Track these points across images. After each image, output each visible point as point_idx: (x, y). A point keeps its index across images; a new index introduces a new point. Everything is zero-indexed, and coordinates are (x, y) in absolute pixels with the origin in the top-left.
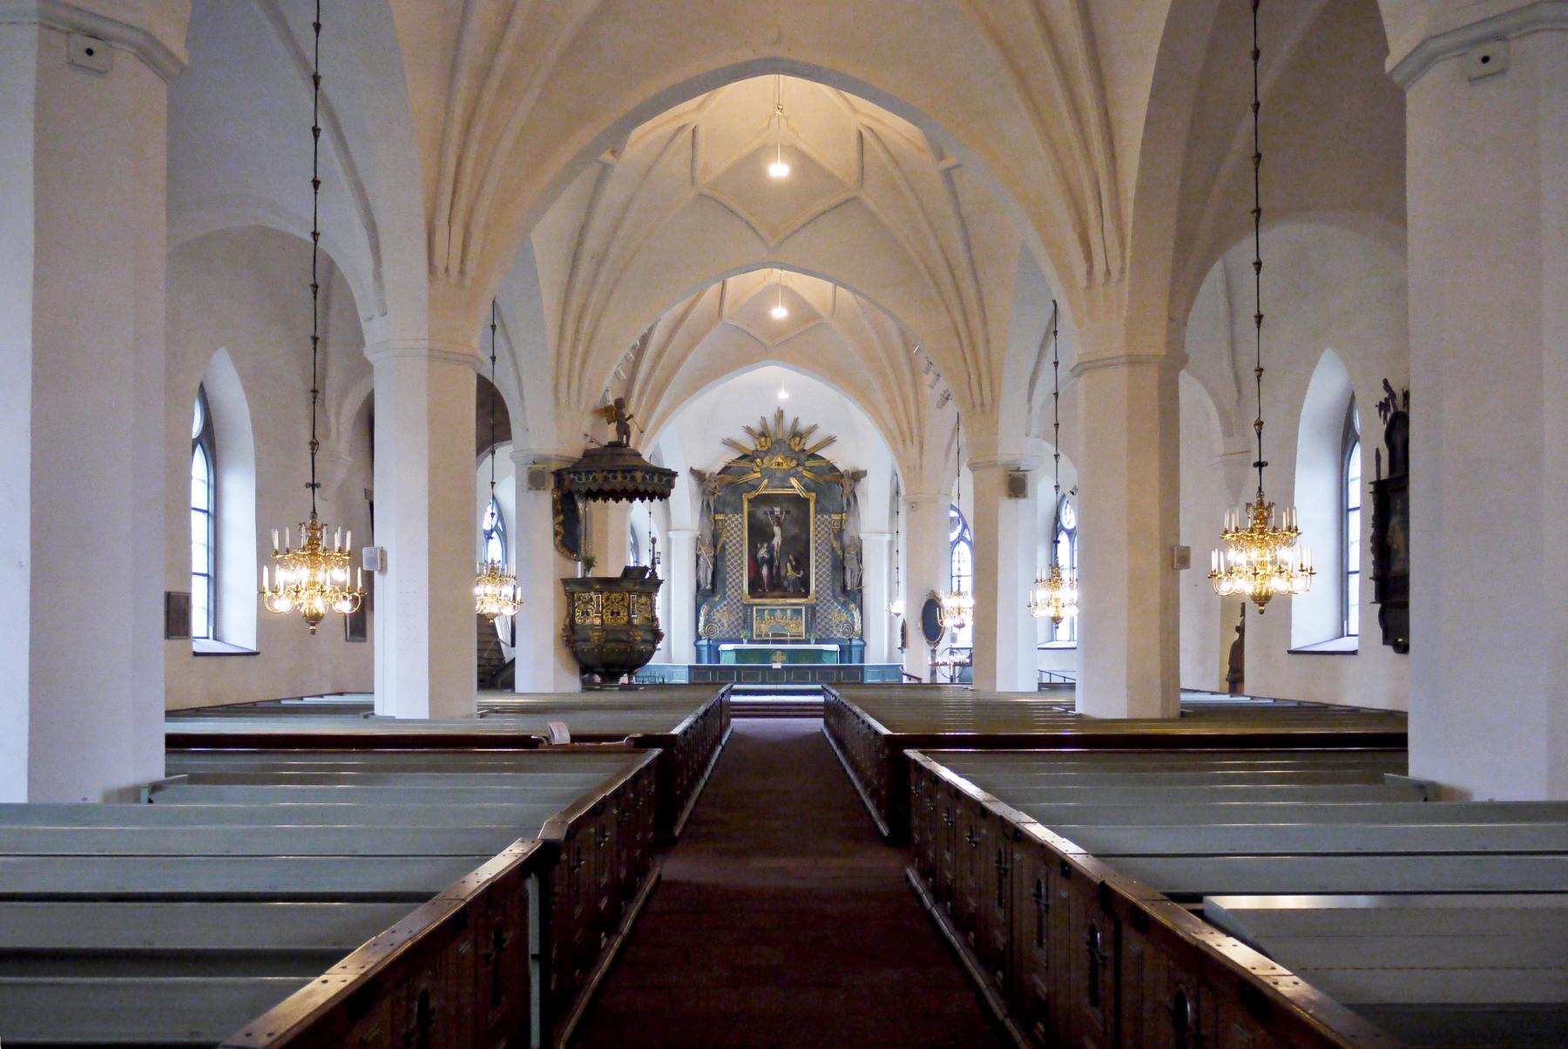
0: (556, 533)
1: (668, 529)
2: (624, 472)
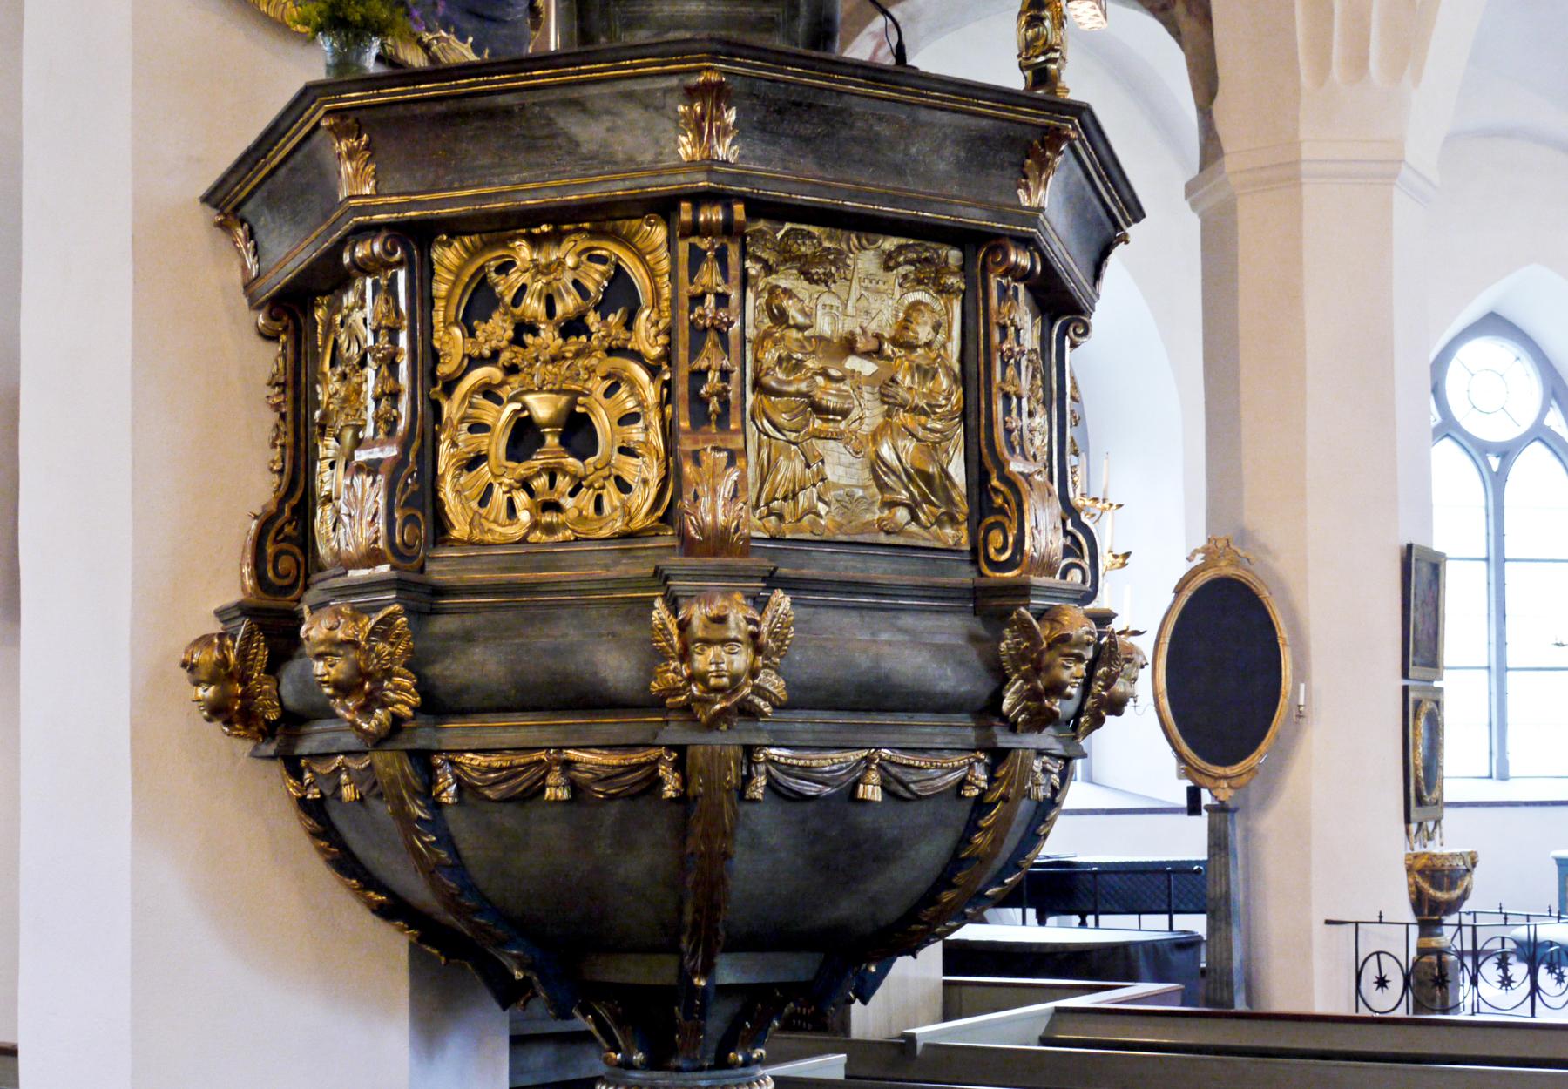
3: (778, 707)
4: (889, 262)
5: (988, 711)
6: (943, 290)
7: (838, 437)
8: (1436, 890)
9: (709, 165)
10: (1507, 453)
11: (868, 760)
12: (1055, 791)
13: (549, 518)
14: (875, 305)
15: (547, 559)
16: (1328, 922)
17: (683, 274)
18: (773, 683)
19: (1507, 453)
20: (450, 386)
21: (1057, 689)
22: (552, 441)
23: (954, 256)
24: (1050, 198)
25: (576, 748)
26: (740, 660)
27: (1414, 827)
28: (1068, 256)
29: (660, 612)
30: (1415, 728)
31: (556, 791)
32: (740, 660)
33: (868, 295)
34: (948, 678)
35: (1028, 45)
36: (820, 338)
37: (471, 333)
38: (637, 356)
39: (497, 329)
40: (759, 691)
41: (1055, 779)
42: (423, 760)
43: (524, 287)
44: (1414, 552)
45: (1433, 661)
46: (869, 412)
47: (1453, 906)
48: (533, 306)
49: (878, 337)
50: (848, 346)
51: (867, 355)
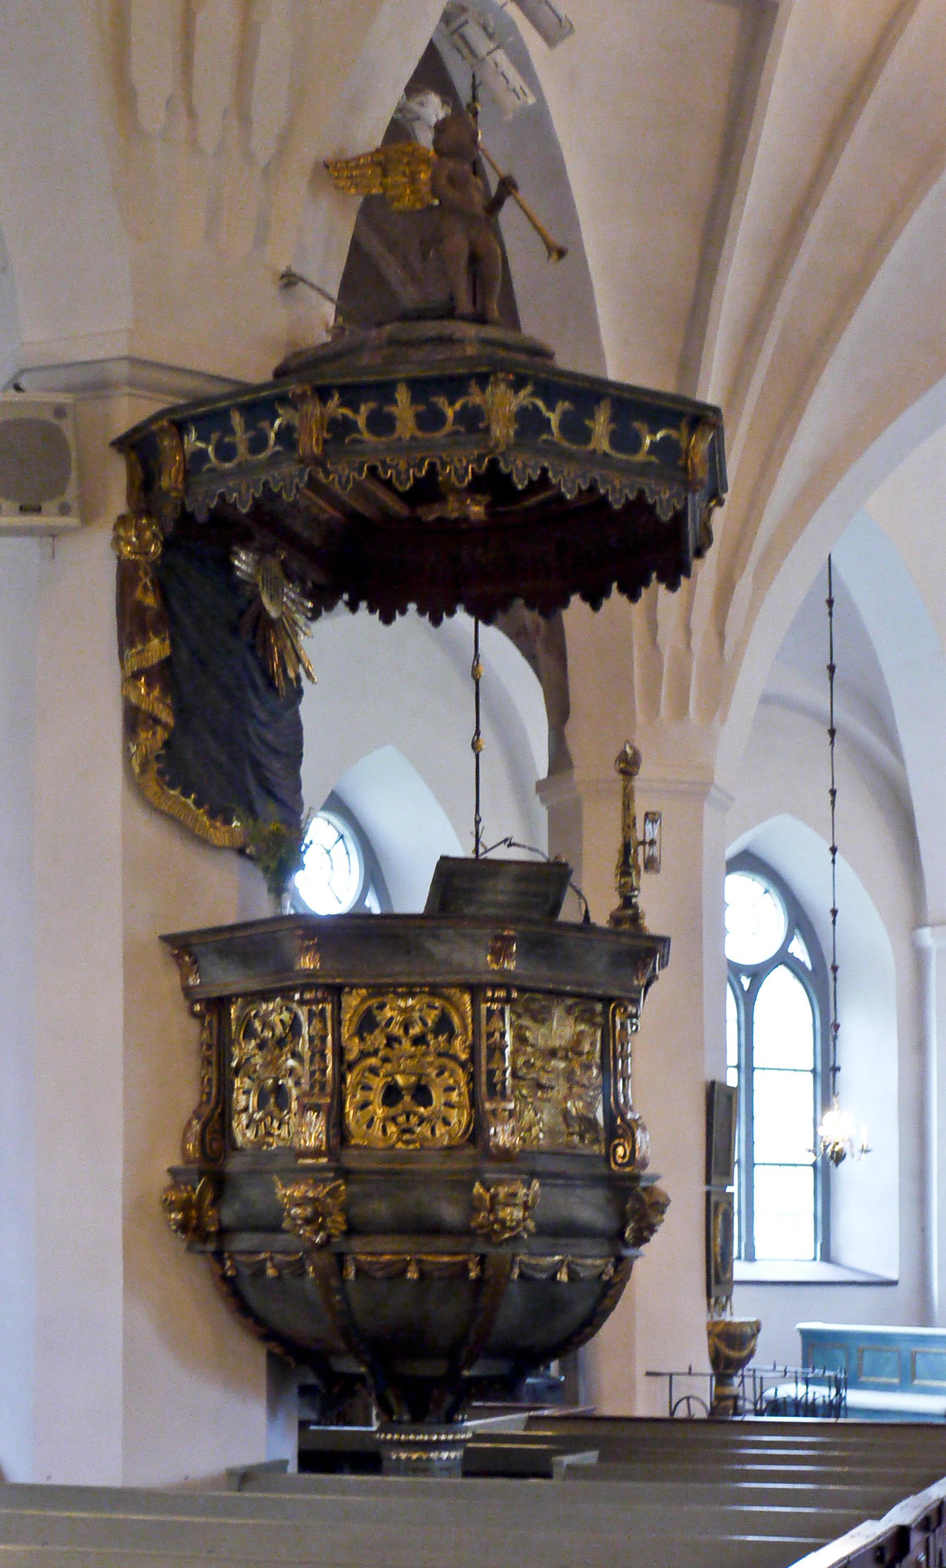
0: (134, 720)
1: (918, 919)
2: (421, 388)
4: (569, 1011)
6: (593, 1024)
8: (730, 1350)
9: (503, 972)
10: (758, 973)
11: (562, 1262)
13: (407, 1137)
15: (407, 1157)
16: (649, 1374)
17: (483, 1021)
18: (531, 1225)
19: (758, 973)
20: (351, 1066)
22: (407, 1098)
23: (599, 1007)
25: (426, 1253)
26: (518, 1214)
27: (713, 1301)
29: (478, 1188)
30: (715, 1221)
31: (412, 1274)
32: (518, 1214)
35: (621, 886)
37: (362, 1039)
38: (454, 1058)
39: (377, 1039)
40: (525, 1229)
42: (340, 1259)
43: (392, 1018)
44: (716, 1087)
46: (561, 1089)
47: (742, 1363)
48: (397, 1030)
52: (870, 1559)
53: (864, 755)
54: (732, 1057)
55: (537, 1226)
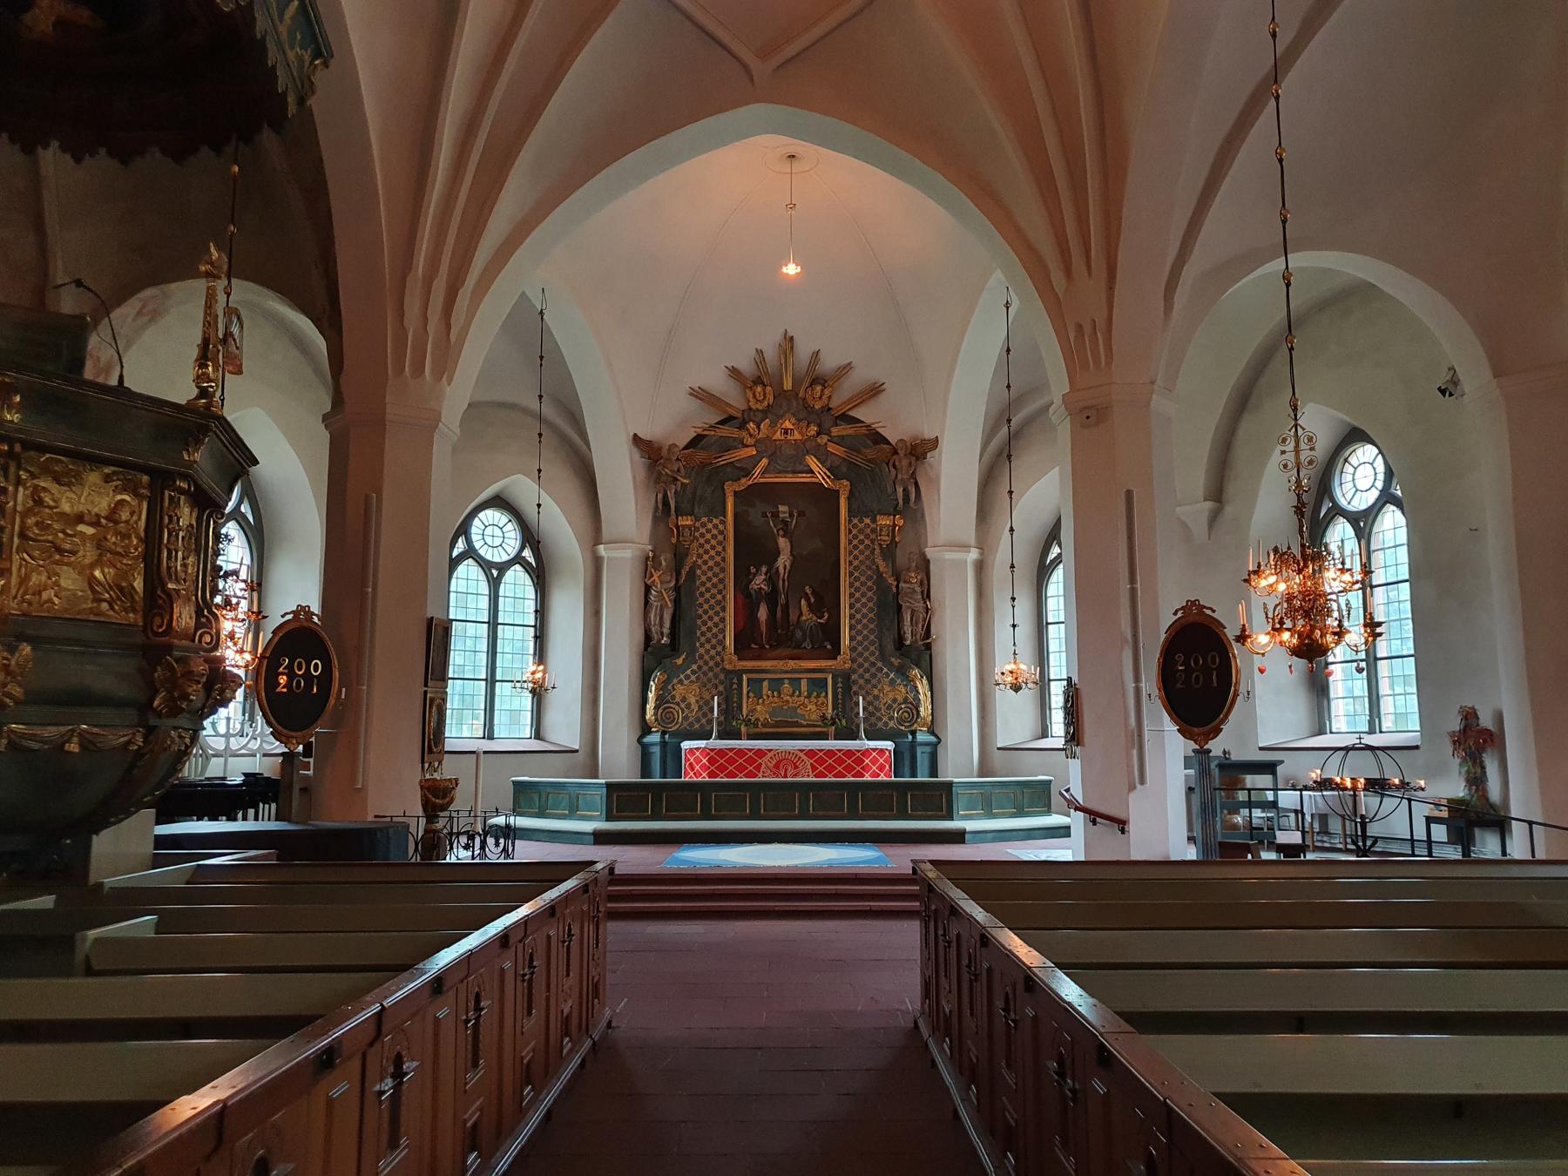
3: (17, 702)
5: (145, 708)
6: (136, 495)
7: (67, 564)
10: (503, 568)
12: (187, 747)
14: (97, 499)
18: (17, 691)
19: (503, 568)
21: (185, 697)
23: (145, 478)
24: (200, 457)
28: (210, 482)
33: (94, 495)
34: (123, 690)
35: (198, 377)
36: (63, 514)
41: (187, 741)
45: (443, 678)
46: (88, 554)
47: (444, 808)
49: (97, 515)
50: (80, 519)
51: (91, 524)
52: (498, 944)
53: (564, 440)
54: (970, 825)
55: (26, 693)
